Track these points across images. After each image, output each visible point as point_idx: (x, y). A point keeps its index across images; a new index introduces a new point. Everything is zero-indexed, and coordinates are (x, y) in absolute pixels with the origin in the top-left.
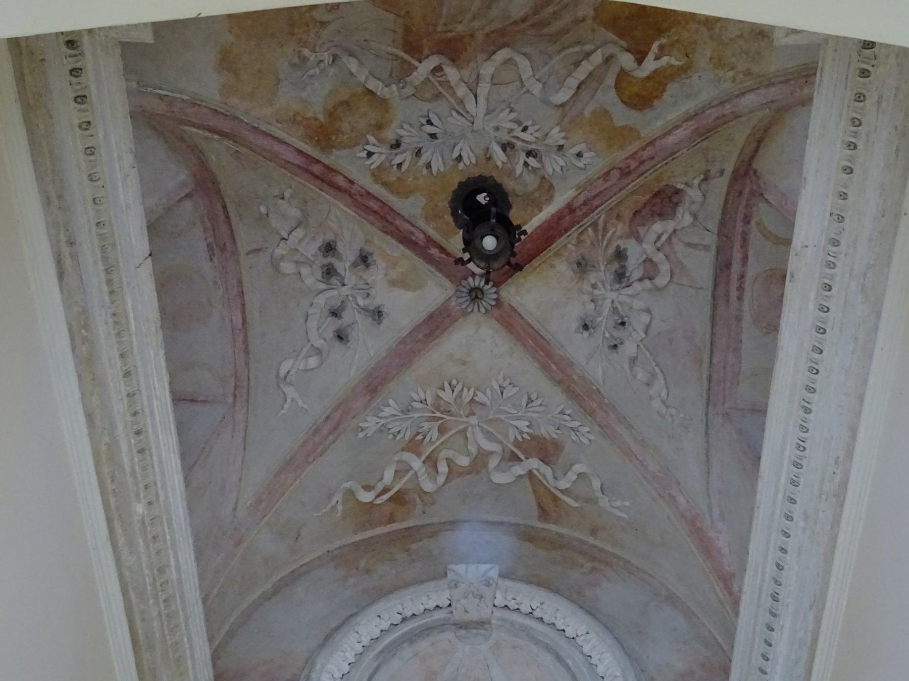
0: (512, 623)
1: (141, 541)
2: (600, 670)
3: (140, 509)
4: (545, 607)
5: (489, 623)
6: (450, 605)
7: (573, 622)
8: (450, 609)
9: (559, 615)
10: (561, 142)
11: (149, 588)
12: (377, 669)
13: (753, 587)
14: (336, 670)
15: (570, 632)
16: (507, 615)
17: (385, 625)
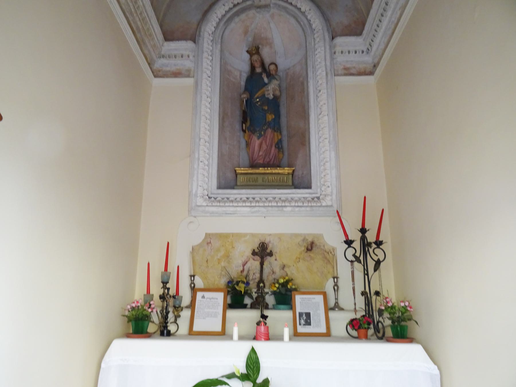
2: (314, 26)
17: (227, 8)
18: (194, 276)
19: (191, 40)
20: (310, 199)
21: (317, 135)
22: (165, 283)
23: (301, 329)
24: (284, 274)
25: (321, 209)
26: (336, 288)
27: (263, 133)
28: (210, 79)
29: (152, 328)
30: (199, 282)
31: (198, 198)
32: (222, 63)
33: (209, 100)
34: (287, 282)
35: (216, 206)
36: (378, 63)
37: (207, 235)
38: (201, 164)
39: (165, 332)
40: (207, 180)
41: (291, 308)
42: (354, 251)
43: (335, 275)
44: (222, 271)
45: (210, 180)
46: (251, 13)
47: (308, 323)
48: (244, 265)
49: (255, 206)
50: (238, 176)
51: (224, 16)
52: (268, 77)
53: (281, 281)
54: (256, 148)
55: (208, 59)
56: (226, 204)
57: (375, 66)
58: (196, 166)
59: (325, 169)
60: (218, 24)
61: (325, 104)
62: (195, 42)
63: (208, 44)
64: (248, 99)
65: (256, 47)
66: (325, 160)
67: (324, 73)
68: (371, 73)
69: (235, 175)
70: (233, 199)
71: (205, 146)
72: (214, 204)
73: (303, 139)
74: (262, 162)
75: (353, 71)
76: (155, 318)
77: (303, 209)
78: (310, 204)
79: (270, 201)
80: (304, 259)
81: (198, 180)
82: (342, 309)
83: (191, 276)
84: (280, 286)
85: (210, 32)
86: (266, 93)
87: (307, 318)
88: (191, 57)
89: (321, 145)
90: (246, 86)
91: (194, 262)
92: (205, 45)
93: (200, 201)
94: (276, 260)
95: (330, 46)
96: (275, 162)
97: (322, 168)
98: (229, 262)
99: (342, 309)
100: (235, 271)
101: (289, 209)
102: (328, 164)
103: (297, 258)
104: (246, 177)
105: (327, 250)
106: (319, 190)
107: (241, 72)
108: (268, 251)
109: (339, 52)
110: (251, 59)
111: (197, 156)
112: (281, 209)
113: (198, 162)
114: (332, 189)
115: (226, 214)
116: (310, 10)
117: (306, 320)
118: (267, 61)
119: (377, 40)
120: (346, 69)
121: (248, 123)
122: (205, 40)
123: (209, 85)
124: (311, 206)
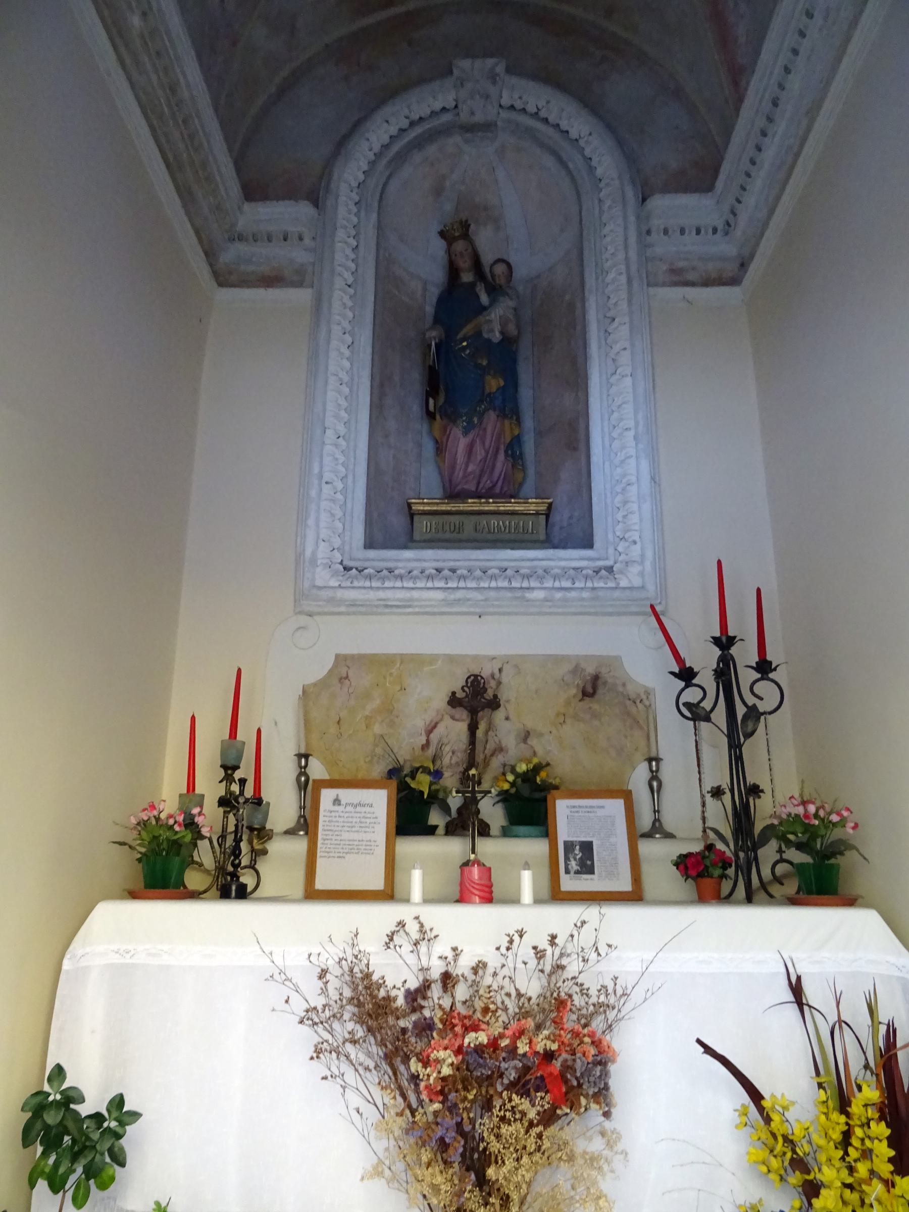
1: (146, 59)
2: (599, 172)
3: (136, 21)
5: (496, 125)
6: (456, 107)
7: (578, 123)
10: (591, 138)
11: (166, 109)
12: (389, 177)
13: (757, 89)
16: (513, 115)
17: (393, 130)
18: (306, 756)
19: (308, 199)
20: (590, 572)
21: (606, 423)
22: (229, 769)
23: (568, 883)
24: (528, 754)
26: (655, 784)
27: (476, 420)
28: (351, 291)
29: (193, 879)
30: (317, 770)
31: (318, 570)
34: (537, 769)
35: (364, 588)
36: (752, 256)
37: (340, 659)
38: (326, 489)
39: (234, 888)
40: (340, 525)
41: (546, 835)
42: (701, 694)
43: (653, 754)
44: (376, 746)
45: (350, 496)
47: (587, 867)
48: (429, 732)
49: (458, 588)
50: (416, 518)
51: (385, 147)
53: (522, 768)
56: (387, 584)
57: (742, 265)
58: (313, 493)
59: (625, 502)
60: (372, 164)
61: (625, 349)
62: (316, 205)
63: (349, 212)
64: (441, 341)
66: (624, 481)
67: (623, 279)
68: (734, 281)
70: (403, 571)
71: (336, 446)
72: (356, 584)
73: (573, 437)
74: (474, 489)
75: (691, 276)
76: (205, 854)
77: (573, 594)
78: (589, 584)
79: (493, 577)
80: (576, 717)
81: (317, 526)
82: (669, 836)
83: (300, 756)
84: (519, 781)
85: (354, 184)
86: (485, 328)
87: (585, 857)
88: (307, 241)
89: (616, 444)
91: (307, 723)
92: (342, 211)
93: (322, 576)
94: (507, 718)
95: (638, 217)
96: (505, 489)
97: (619, 498)
98: (392, 724)
99: (669, 836)
100: (407, 745)
101: (539, 595)
102: (633, 489)
103: (558, 715)
104: (435, 520)
105: (633, 696)
106: (611, 551)
107: (425, 283)
108: (490, 694)
110: (449, 251)
111: (316, 470)
112: (518, 594)
113: (320, 485)
114: (642, 549)
115: (387, 606)
116: (590, 134)
117: (581, 858)
118: (487, 258)
119: (750, 200)
120: (673, 271)
121: (442, 399)
122: (342, 199)
123: (349, 303)
124: (594, 589)
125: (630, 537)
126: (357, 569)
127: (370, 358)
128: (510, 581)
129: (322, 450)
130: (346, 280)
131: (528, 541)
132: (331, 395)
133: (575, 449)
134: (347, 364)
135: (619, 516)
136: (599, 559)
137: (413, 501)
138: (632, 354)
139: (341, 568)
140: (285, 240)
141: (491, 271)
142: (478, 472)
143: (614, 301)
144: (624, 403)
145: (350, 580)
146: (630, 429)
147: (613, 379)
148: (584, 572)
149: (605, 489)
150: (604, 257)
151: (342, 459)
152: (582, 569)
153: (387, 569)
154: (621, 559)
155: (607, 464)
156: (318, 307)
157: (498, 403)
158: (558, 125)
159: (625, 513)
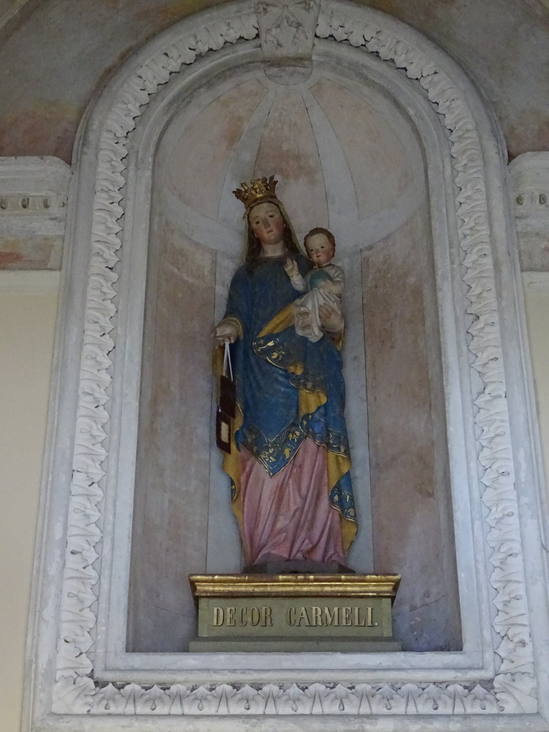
0: (339, 61)
2: (449, 121)
4: (382, 37)
5: (310, 59)
6: (258, 36)
8: (257, 41)
9: (400, 48)
14: (119, 129)
15: (413, 72)
16: (333, 48)
17: (175, 65)
25: (501, 724)
27: (287, 452)
28: (114, 276)
31: (57, 687)
32: (155, 227)
33: (109, 342)
35: (124, 715)
38: (72, 561)
40: (92, 616)
45: (106, 572)
46: (251, 79)
49: (265, 716)
50: (203, 603)
52: (303, 272)
54: (267, 506)
55: (110, 212)
58: (53, 570)
60: (146, 107)
64: (237, 340)
65: (264, 180)
66: (503, 550)
67: (488, 262)
69: (188, 598)
70: (182, 688)
73: (427, 475)
74: (286, 555)
78: (459, 710)
79: (316, 698)
85: (121, 133)
86: (298, 322)
88: (55, 210)
90: (231, 298)
92: (103, 168)
93: (64, 698)
95: (504, 181)
97: (496, 575)
102: (516, 564)
104: (230, 606)
106: (489, 656)
107: (214, 253)
109: (532, 199)
110: (248, 216)
111: (58, 534)
113: (63, 556)
118: (301, 225)
121: (238, 422)
124: (466, 716)
125: (515, 635)
126: (114, 683)
127: (138, 369)
128: (342, 703)
129: (67, 506)
130: (106, 261)
131: (367, 639)
132: (82, 422)
133: (430, 495)
134: (106, 377)
135: (498, 602)
136: (470, 668)
137: (199, 577)
138: (506, 366)
139: (91, 683)
140: (24, 207)
141: (305, 244)
142: (292, 526)
143: (477, 292)
144: (497, 435)
145: (104, 702)
146: (517, 555)
147: (481, 401)
148: (451, 688)
149: (476, 561)
150: (460, 231)
151: (96, 515)
152: (447, 684)
153: (159, 684)
154: (503, 668)
155: (477, 524)
156: (68, 293)
157: (318, 428)
158: (392, 60)
159: (507, 598)
